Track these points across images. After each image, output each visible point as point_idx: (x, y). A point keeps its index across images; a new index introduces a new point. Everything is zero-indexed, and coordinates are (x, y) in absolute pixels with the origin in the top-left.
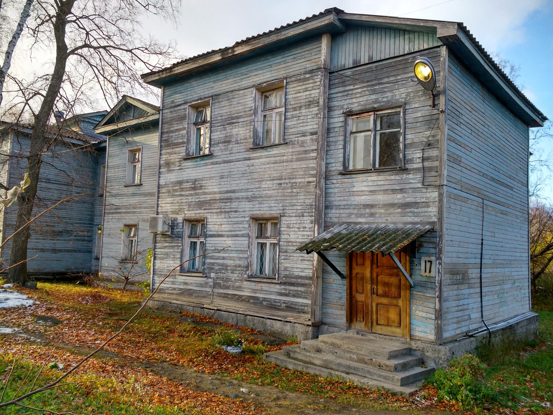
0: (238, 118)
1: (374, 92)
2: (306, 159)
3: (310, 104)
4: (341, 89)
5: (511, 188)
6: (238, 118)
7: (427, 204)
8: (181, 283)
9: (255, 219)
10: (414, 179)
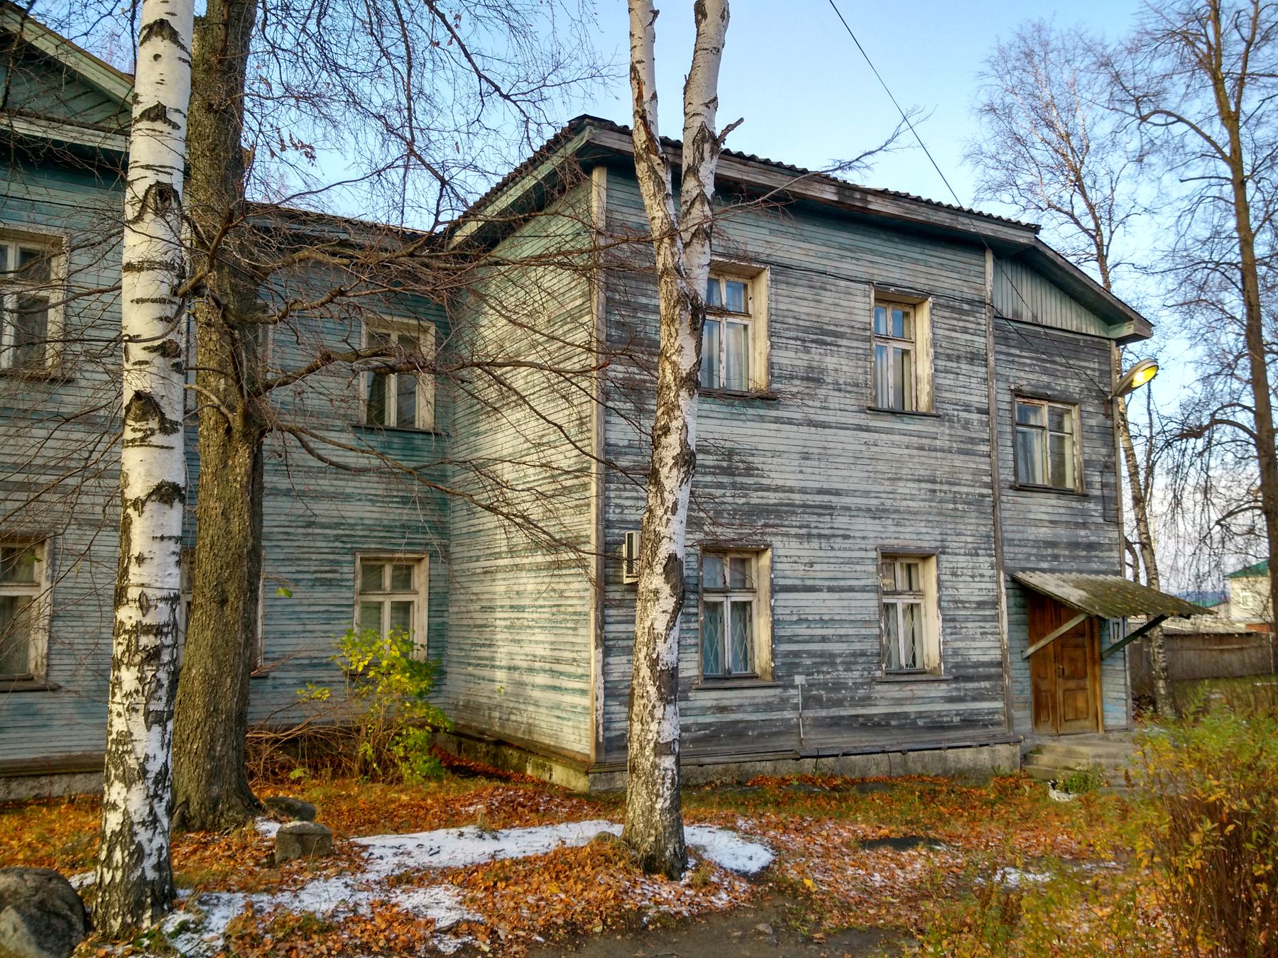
0: (842, 335)
1: (1045, 372)
2: (974, 453)
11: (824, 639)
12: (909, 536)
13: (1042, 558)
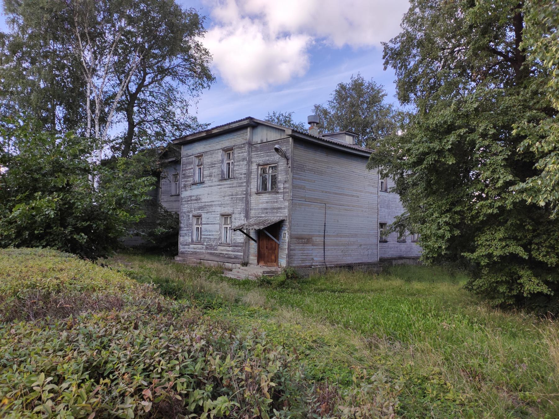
0: (215, 164)
1: (268, 156)
2: (242, 186)
3: (244, 159)
4: (256, 153)
5: (358, 197)
6: (215, 164)
7: (284, 208)
8: (192, 248)
9: (222, 215)
10: (280, 196)
11: (210, 235)
12: (227, 210)
13: (263, 213)
